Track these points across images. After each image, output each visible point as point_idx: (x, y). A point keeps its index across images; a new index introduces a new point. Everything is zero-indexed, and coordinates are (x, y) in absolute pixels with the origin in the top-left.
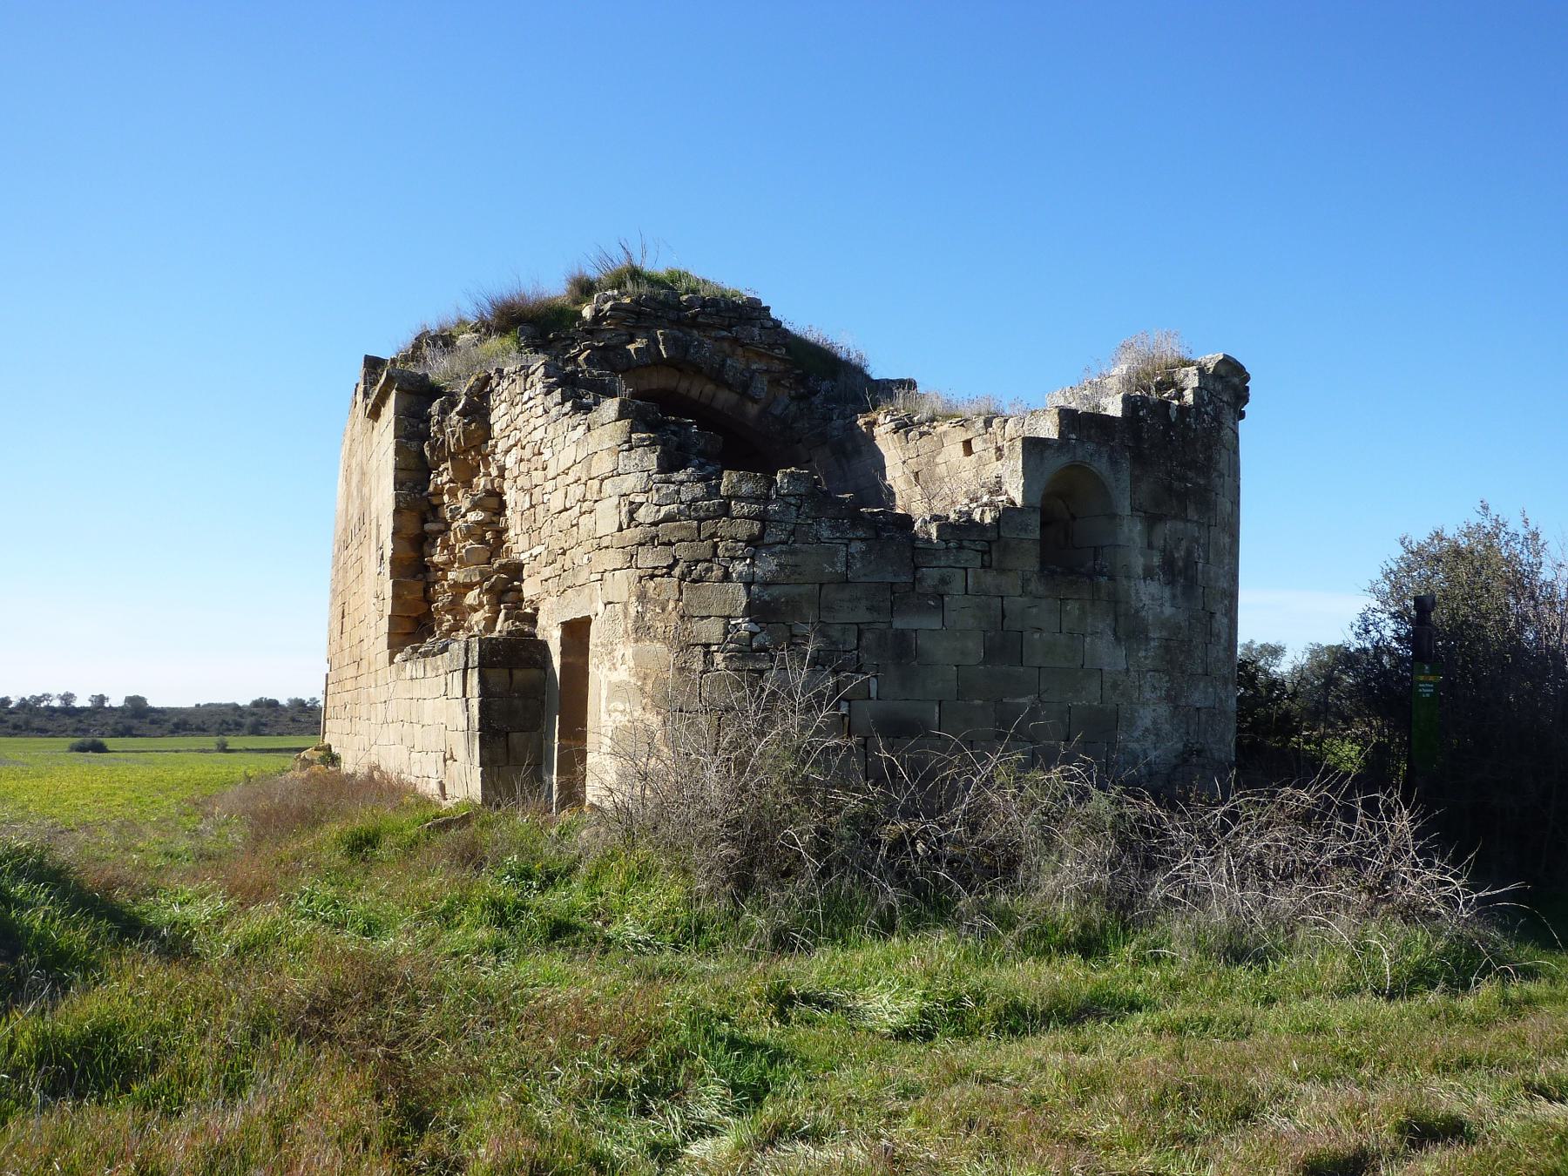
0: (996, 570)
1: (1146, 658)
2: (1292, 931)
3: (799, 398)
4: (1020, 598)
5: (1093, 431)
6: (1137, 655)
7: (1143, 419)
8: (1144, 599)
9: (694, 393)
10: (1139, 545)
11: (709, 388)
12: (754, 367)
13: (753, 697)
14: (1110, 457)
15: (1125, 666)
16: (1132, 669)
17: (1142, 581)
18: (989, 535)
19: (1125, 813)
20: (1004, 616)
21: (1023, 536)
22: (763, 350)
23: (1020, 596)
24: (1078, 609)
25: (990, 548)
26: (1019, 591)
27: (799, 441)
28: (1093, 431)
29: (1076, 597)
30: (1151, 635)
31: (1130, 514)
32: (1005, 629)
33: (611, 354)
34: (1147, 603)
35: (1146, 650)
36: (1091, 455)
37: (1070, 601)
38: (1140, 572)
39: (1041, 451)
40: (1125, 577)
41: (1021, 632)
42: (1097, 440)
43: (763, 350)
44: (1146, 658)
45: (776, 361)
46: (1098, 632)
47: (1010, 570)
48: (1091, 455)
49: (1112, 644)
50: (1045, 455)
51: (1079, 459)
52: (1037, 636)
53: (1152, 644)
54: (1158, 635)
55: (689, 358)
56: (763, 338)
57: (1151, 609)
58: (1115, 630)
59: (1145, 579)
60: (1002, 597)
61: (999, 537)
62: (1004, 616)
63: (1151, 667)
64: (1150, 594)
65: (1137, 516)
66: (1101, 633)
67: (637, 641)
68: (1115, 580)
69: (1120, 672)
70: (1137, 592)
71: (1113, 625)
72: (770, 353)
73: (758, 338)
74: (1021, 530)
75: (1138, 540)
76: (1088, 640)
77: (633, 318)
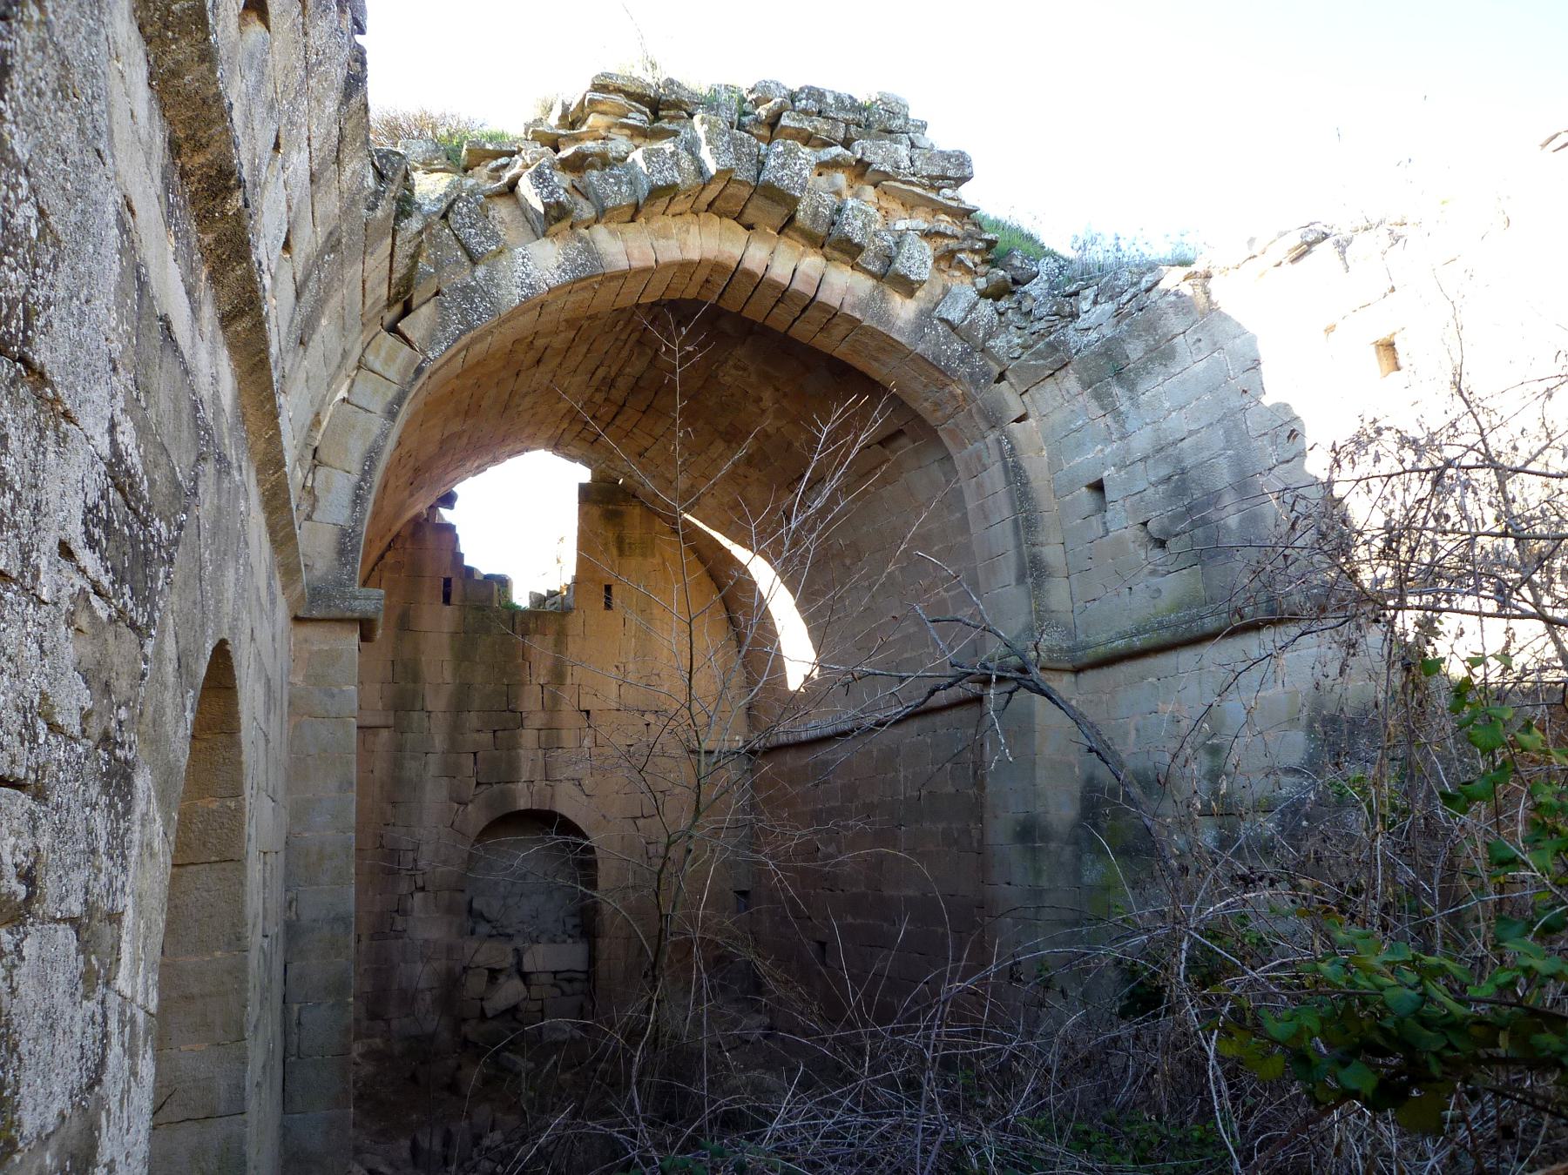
2: (81, 194)
3: (995, 293)
9: (780, 272)
11: (812, 263)
12: (901, 225)
13: (943, 975)
19: (1429, 1159)
22: (919, 190)
27: (1001, 377)
33: (594, 176)
43: (919, 190)
45: (943, 217)
55: (765, 176)
56: (918, 163)
72: (932, 195)
73: (906, 163)
77: (645, 114)
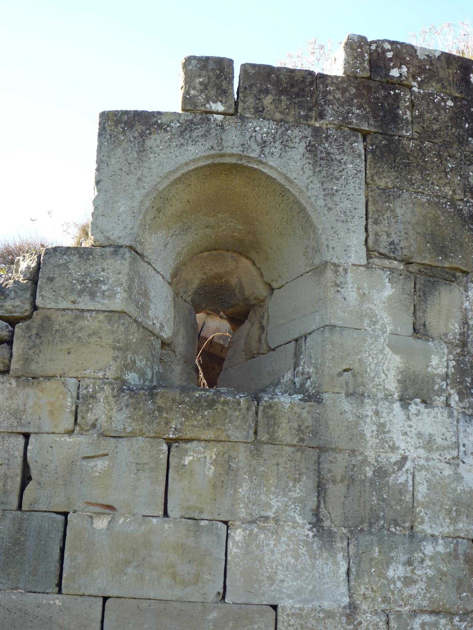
0: (18, 377)
1: (408, 581)
4: (68, 439)
5: (268, 100)
6: (382, 575)
7: (400, 83)
8: (403, 446)
10: (389, 329)
14: (311, 149)
15: (346, 600)
16: (364, 607)
17: (397, 406)
18: (8, 304)
20: (26, 479)
21: (85, 303)
23: (70, 433)
24: (215, 463)
25: (12, 334)
26: (69, 423)
28: (268, 100)
29: (210, 434)
30: (426, 528)
31: (364, 261)
32: (24, 507)
34: (412, 454)
35: (409, 563)
36: (264, 144)
37: (188, 446)
38: (392, 385)
39: (142, 135)
40: (348, 395)
41: (66, 514)
42: (278, 116)
44: (408, 581)
46: (266, 519)
47: (49, 378)
48: (264, 144)
49: (307, 544)
50: (149, 143)
51: (235, 151)
52: (101, 523)
53: (429, 549)
54: (447, 529)
57: (422, 468)
58: (316, 513)
59: (405, 402)
60: (27, 436)
61: (35, 308)
62: (26, 479)
63: (425, 603)
64: (419, 435)
65: (383, 268)
66: (277, 521)
67: (184, 579)
68: (319, 401)
69: (330, 615)
70: (382, 428)
71: (312, 502)
74: (80, 293)
75: (385, 318)
76: (238, 535)
